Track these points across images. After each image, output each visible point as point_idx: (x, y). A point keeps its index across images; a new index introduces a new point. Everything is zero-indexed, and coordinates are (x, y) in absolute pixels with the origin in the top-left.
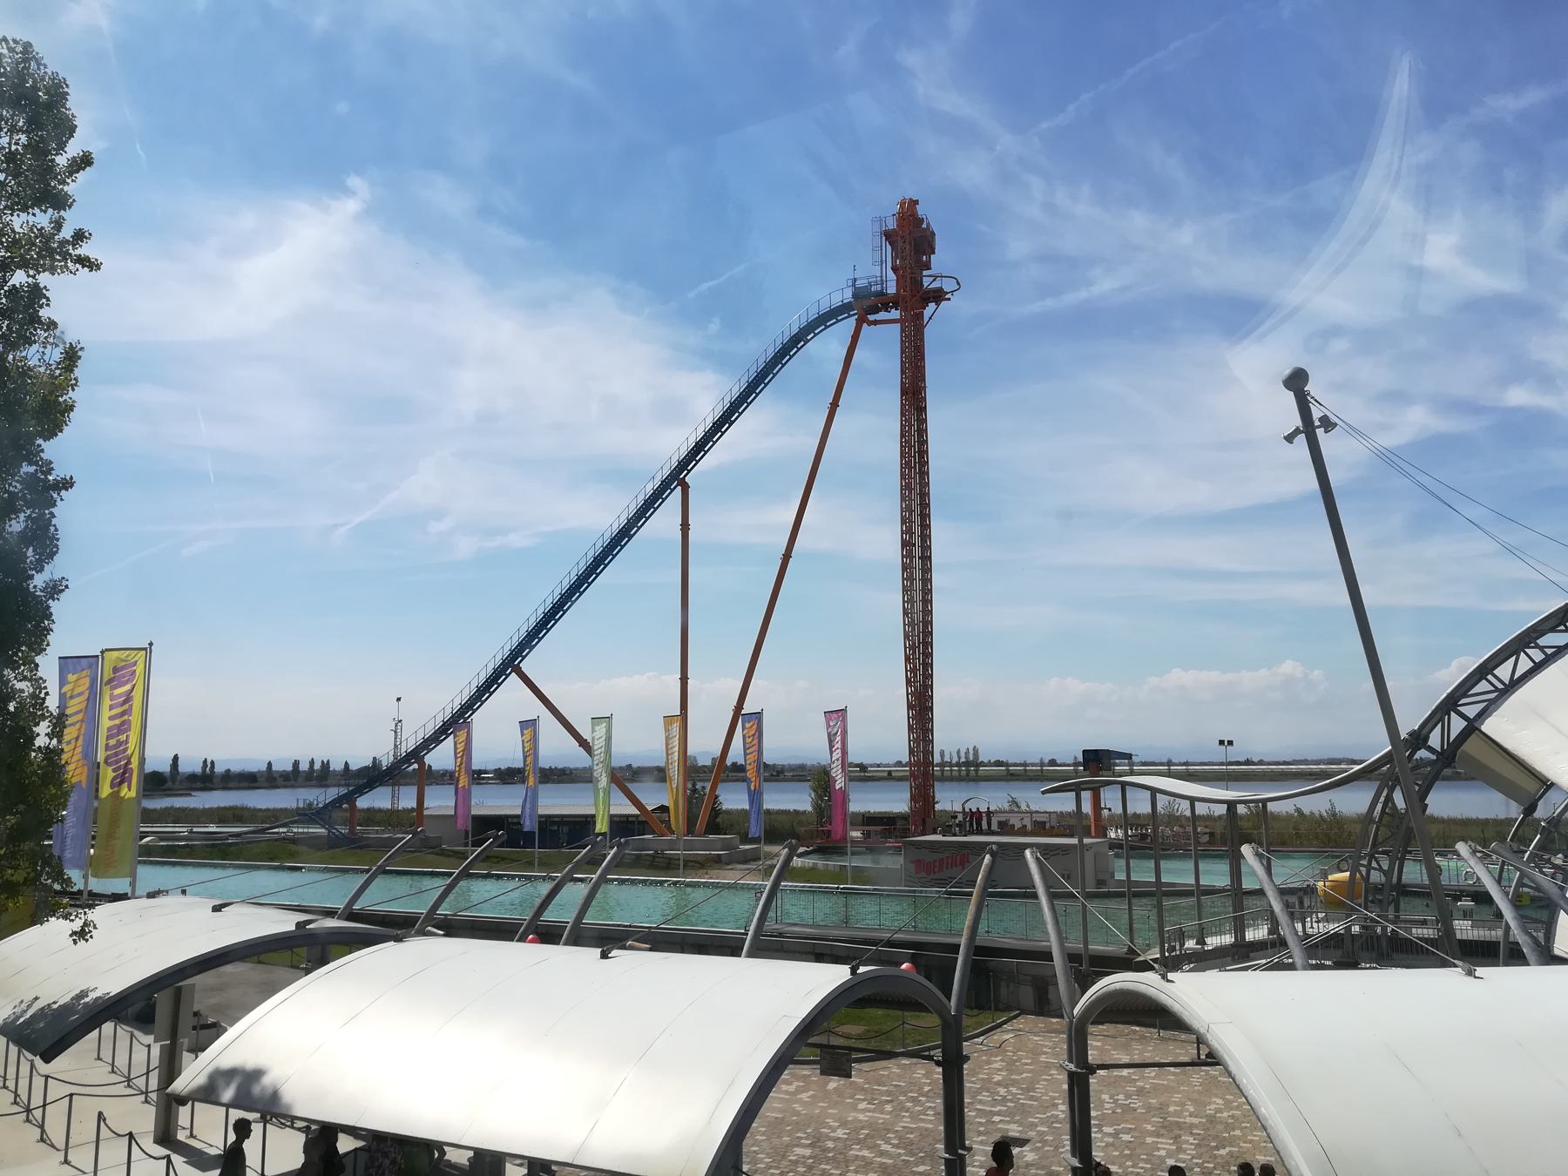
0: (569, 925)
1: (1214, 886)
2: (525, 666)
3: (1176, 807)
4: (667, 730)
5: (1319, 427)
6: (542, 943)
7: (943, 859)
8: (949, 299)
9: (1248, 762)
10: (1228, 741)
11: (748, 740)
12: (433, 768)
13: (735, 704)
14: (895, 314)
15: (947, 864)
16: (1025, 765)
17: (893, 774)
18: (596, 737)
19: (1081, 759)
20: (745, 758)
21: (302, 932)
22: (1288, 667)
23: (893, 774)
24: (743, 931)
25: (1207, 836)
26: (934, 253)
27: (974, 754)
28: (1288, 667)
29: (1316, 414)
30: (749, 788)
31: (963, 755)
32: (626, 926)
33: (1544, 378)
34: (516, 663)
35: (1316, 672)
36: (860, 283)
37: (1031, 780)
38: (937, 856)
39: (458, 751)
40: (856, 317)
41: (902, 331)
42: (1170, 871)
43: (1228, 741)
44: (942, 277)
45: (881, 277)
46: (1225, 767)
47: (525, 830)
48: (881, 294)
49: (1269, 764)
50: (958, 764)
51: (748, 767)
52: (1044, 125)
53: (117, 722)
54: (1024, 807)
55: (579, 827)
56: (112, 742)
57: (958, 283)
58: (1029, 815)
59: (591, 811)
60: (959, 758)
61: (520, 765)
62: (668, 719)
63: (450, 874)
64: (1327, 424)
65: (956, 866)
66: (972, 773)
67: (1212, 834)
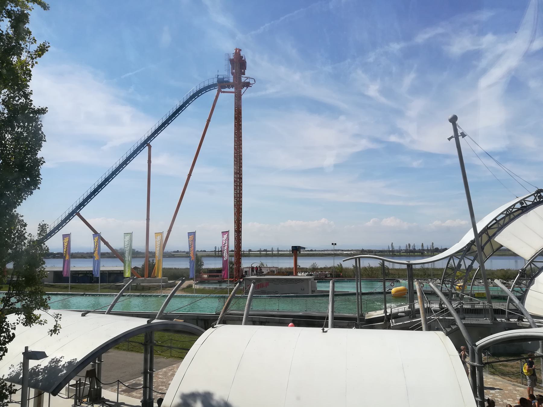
0: (158, 314)
1: (349, 292)
2: (82, 212)
3: (316, 265)
5: (460, 136)
6: (295, 326)
8: (251, 87)
9: (311, 251)
10: (335, 244)
11: (65, 244)
13: (168, 229)
14: (233, 90)
15: (261, 286)
18: (65, 242)
19: (291, 250)
20: (189, 248)
21: (149, 325)
22: (323, 220)
24: (215, 313)
25: (330, 275)
26: (246, 69)
28: (323, 220)
29: (459, 131)
30: (190, 260)
33: (401, 133)
34: (77, 212)
35: (332, 222)
37: (245, 256)
39: (65, 245)
40: (218, 89)
41: (235, 96)
42: (320, 287)
43: (335, 244)
44: (250, 78)
45: (228, 75)
46: (333, 252)
47: (64, 276)
48: (228, 82)
49: (317, 251)
50: (218, 251)
51: (191, 252)
54: (265, 266)
55: (118, 276)
57: (255, 81)
58: (269, 268)
59: (122, 268)
63: (117, 295)
64: (463, 135)
65: (264, 287)
66: (217, 255)
67: (331, 274)
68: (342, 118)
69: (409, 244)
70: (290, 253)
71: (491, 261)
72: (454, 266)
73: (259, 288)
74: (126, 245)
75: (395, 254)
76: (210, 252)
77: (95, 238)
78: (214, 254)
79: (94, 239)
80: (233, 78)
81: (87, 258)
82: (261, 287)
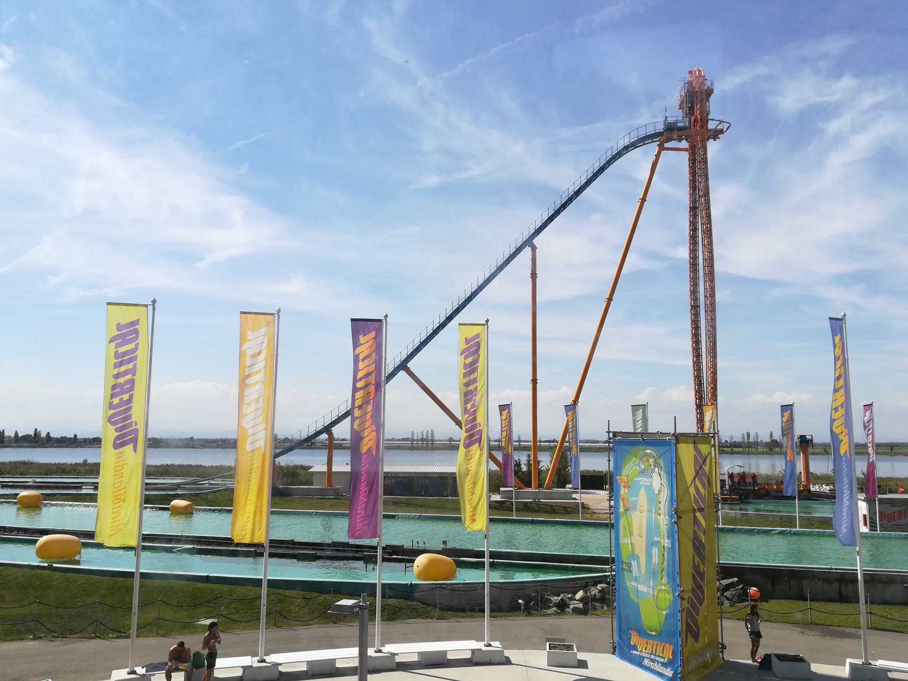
2: (409, 365)
4: (634, 415)
11: (504, 422)
12: (78, 437)
20: (502, 434)
27: (431, 434)
31: (430, 435)
32: (829, 569)
36: (670, 120)
38: (897, 509)
50: (417, 440)
52: (445, 74)
60: (423, 436)
66: (430, 445)
68: (596, 217)
69: (747, 432)
71: (892, 465)
74: (504, 427)
75: (724, 450)
77: (785, 414)
78: (410, 445)
80: (358, 658)
82: (905, 517)
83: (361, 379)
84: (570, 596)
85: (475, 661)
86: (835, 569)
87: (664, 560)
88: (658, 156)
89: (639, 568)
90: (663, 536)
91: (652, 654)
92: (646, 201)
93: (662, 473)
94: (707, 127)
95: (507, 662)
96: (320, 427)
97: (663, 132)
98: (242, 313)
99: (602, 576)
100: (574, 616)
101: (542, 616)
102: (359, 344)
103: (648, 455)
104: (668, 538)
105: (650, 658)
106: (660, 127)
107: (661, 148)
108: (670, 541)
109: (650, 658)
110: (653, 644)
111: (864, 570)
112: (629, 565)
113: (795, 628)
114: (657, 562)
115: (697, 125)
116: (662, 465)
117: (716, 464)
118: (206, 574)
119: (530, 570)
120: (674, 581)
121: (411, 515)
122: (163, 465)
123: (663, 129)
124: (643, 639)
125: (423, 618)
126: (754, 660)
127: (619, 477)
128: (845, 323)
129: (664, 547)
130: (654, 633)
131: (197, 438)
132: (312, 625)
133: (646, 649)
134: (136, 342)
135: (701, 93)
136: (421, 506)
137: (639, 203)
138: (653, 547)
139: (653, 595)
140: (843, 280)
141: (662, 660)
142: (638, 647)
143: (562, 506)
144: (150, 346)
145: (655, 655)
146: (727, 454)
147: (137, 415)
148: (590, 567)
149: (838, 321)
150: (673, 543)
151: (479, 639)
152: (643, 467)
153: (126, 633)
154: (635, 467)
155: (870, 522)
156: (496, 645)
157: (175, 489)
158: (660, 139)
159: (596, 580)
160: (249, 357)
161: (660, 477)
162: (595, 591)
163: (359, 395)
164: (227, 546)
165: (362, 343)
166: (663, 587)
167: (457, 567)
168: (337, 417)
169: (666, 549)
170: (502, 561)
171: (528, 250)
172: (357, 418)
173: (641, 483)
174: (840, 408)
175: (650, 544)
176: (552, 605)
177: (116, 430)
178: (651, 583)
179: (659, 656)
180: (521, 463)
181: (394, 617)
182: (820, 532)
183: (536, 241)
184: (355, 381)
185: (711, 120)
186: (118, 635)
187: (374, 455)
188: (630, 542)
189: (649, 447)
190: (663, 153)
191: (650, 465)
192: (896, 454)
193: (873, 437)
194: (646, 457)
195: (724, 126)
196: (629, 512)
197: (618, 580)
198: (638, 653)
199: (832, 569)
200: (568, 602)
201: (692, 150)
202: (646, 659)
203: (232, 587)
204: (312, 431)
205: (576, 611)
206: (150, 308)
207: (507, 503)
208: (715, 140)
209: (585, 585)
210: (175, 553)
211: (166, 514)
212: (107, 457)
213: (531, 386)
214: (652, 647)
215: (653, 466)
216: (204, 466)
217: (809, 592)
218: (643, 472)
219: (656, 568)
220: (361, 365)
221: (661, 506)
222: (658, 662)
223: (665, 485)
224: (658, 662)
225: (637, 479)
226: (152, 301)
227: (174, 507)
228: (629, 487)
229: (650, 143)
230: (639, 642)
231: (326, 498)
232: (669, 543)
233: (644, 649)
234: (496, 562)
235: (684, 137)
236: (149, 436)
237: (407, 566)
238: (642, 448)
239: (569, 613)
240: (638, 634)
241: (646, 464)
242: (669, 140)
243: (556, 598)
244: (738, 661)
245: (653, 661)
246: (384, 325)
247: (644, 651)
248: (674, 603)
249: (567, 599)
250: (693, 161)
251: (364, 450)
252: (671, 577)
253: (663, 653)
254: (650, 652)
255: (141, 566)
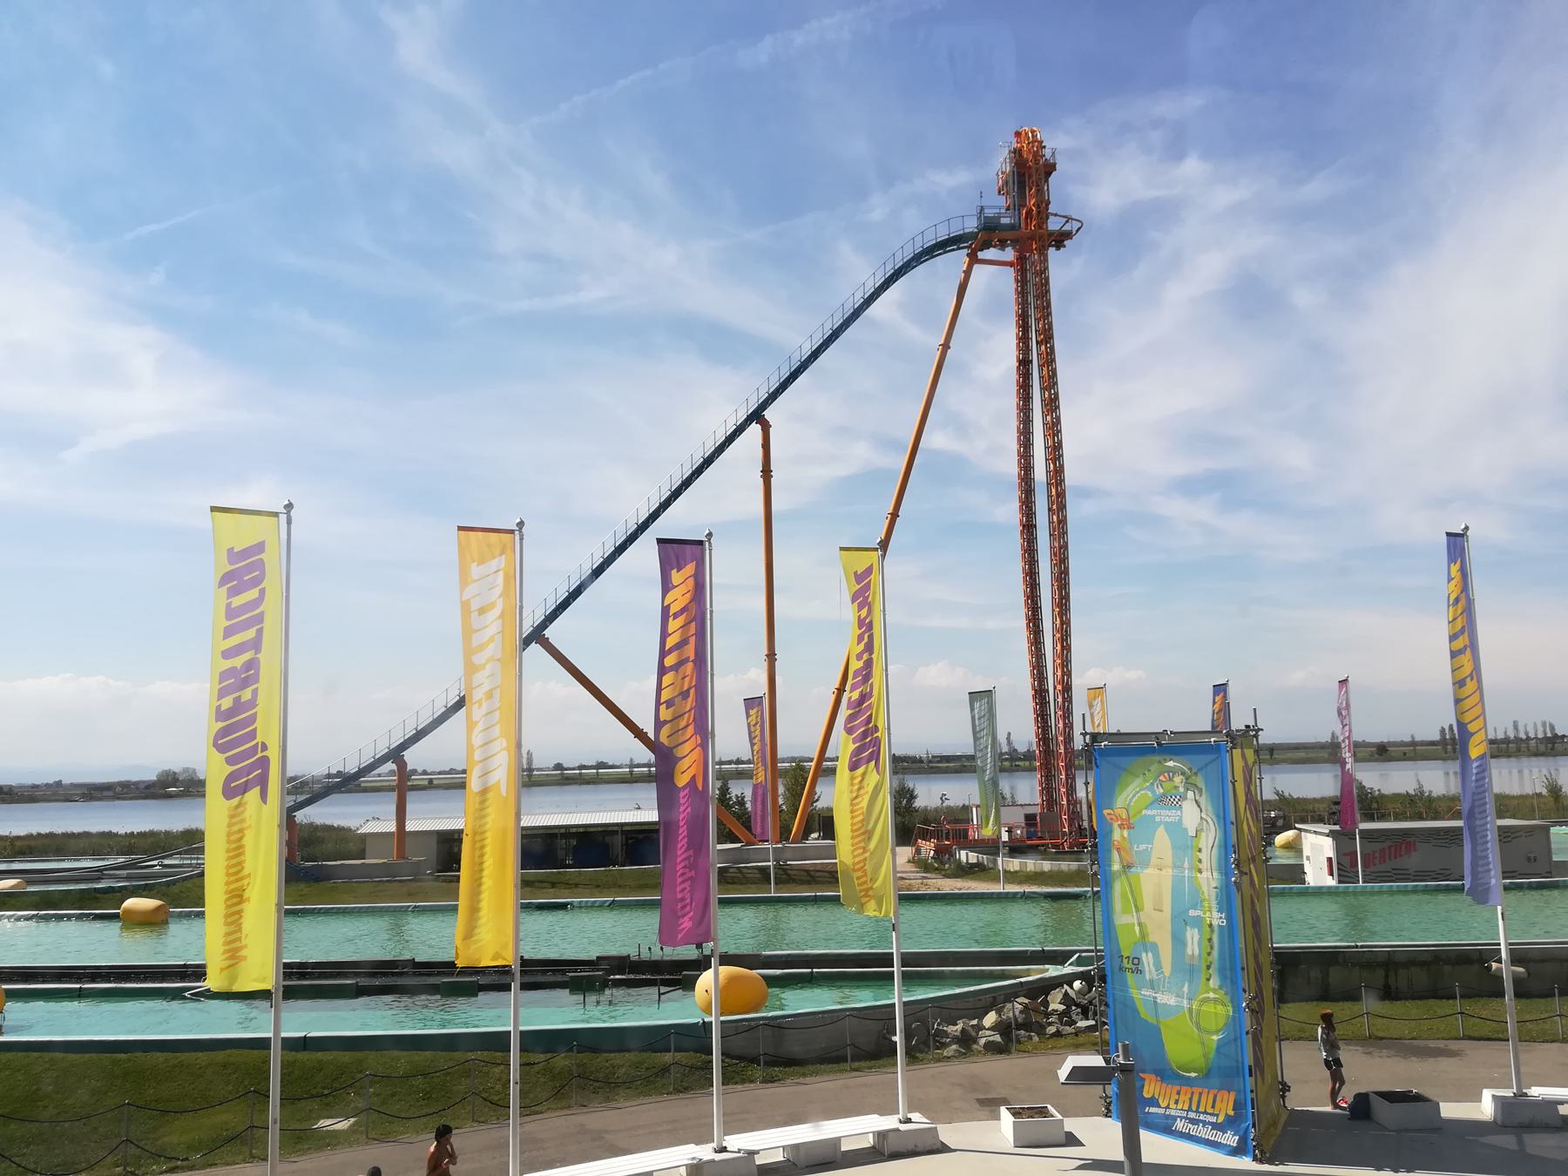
2: (547, 633)
7: (1384, 849)
16: (632, 766)
17: (435, 782)
23: (435, 782)
27: (528, 759)
32: (1353, 947)
36: (989, 212)
53: (238, 662)
56: (227, 703)
61: (971, 752)
62: (750, 703)
70: (650, 771)
72: (1259, 798)
73: (1384, 861)
76: (440, 773)
79: (748, 716)
81: (76, 801)
82: (1390, 859)
83: (671, 651)
84: (975, 1022)
85: (884, 1150)
86: (1362, 947)
87: (1212, 948)
88: (968, 273)
89: (1158, 963)
90: (1210, 907)
91: (1190, 1109)
92: (949, 348)
93: (1203, 800)
94: (1047, 227)
95: (944, 1149)
96: (382, 750)
97: (977, 234)
98: (460, 528)
99: (1017, 983)
100: (989, 1057)
101: (939, 1060)
102: (671, 585)
103: (1172, 771)
104: (1220, 911)
105: (1186, 1118)
106: (971, 225)
107: (973, 259)
108: (1223, 916)
109: (1186, 1118)
110: (1193, 1093)
111: (1511, 944)
112: (1136, 961)
113: (1351, 1048)
114: (1197, 952)
115: (1031, 222)
116: (1202, 785)
117: (1261, 782)
118: (302, 1034)
119: (880, 983)
120: (1234, 983)
121: (595, 902)
122: (32, 835)
123: (977, 228)
124: (1170, 1086)
125: (736, 1083)
126: (1336, 1106)
127: (1109, 811)
128: (1467, 541)
129: (1211, 925)
130: (1193, 1075)
131: (1420, 739)
132: (541, 1113)
133: (1177, 1102)
134: (261, 587)
135: (1037, 170)
136: (576, 885)
137: (939, 352)
138: (1188, 928)
139: (1190, 1010)
140: (1189, 487)
141: (1214, 1119)
142: (1160, 1101)
143: (827, 869)
144: (284, 594)
145: (1197, 1111)
146: (1023, 771)
147: (267, 731)
148: (982, 971)
149: (1458, 538)
150: (1229, 918)
151: (887, 1109)
152: (1162, 791)
153: (187, 1159)
154: (1143, 792)
155: (1339, 869)
156: (919, 1120)
157: (98, 879)
158: (971, 244)
159: (1008, 992)
160: (477, 613)
161: (1199, 806)
162: (1016, 1008)
163: (667, 679)
164: (299, 979)
165: (675, 584)
166: (1212, 995)
167: (769, 987)
168: (415, 731)
169: (1216, 929)
170: (920, 966)
171: (755, 429)
172: (666, 722)
173: (1158, 819)
174: (1468, 680)
175: (1180, 921)
176: (948, 1040)
177: (230, 761)
178: (1186, 989)
179: (1205, 1113)
180: (746, 800)
181: (686, 1084)
182: (1284, 888)
183: (767, 414)
184: (663, 654)
185: (1052, 214)
186: (170, 1165)
187: (700, 789)
188: (1136, 922)
189: (1173, 757)
190: (976, 267)
191: (1176, 787)
192: (1278, 762)
193: (1350, 731)
194: (1166, 774)
195: (1074, 226)
196: (1132, 870)
197: (1114, 989)
198: (1161, 1111)
199: (1357, 947)
200: (973, 1034)
201: (1020, 265)
202: (1179, 1119)
203: (359, 1055)
204: (367, 760)
205: (992, 1048)
206: (283, 518)
207: (731, 870)
208: (1058, 248)
209: (995, 1000)
210: (189, 999)
211: (114, 928)
212: (212, 815)
213: (765, 665)
214: (1191, 1099)
215: (1181, 790)
216: (116, 835)
217: (1365, 986)
218: (1161, 800)
219: (1196, 962)
220: (674, 625)
221: (1204, 856)
222: (1205, 1123)
223: (1209, 820)
224: (1205, 1123)
225: (1149, 812)
226: (285, 507)
227: (128, 912)
228: (1130, 827)
229: (953, 250)
230: (1163, 1092)
231: (397, 880)
232: (1221, 918)
233: (1172, 1102)
234: (816, 972)
235: (1009, 242)
236: (290, 774)
237: (662, 991)
238: (1157, 758)
239: (980, 1052)
240: (1159, 1078)
241: (1168, 785)
242: (986, 245)
243: (955, 1028)
244: (1310, 1109)
245: (1194, 1122)
246: (708, 552)
247: (1173, 1106)
248: (1234, 1021)
249: (970, 1029)
250: (1022, 281)
251: (682, 780)
252: (1228, 974)
253: (1213, 1107)
254: (1186, 1108)
255: (521, 1020)
